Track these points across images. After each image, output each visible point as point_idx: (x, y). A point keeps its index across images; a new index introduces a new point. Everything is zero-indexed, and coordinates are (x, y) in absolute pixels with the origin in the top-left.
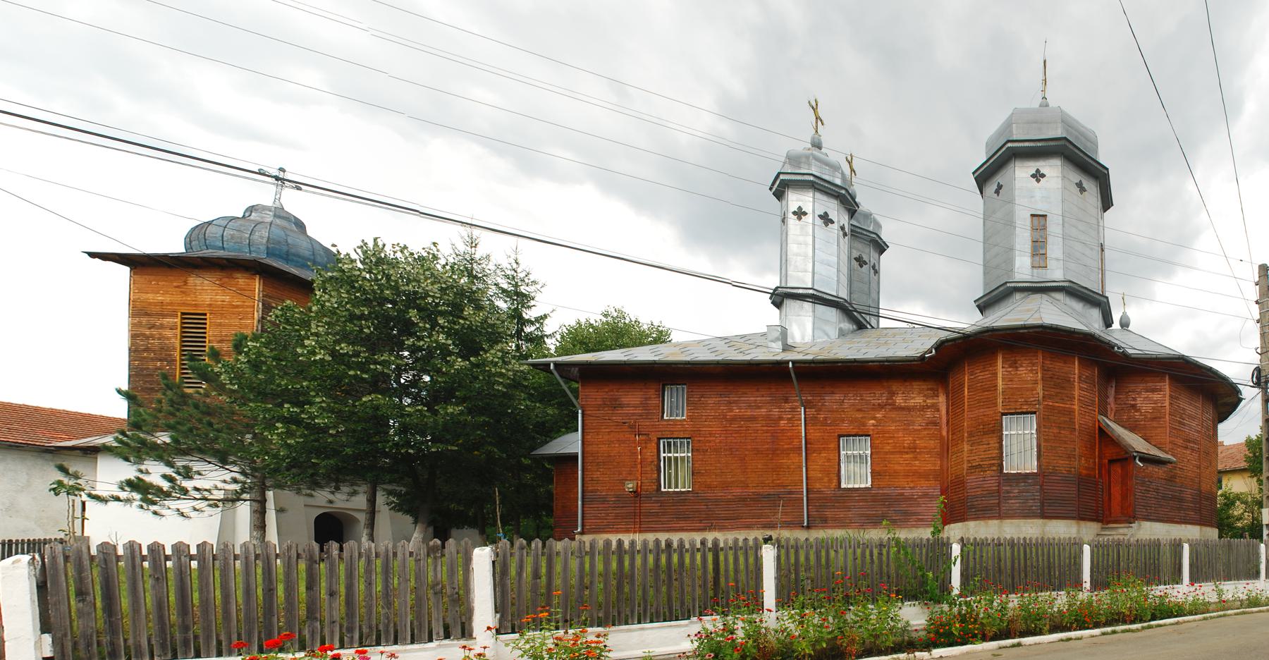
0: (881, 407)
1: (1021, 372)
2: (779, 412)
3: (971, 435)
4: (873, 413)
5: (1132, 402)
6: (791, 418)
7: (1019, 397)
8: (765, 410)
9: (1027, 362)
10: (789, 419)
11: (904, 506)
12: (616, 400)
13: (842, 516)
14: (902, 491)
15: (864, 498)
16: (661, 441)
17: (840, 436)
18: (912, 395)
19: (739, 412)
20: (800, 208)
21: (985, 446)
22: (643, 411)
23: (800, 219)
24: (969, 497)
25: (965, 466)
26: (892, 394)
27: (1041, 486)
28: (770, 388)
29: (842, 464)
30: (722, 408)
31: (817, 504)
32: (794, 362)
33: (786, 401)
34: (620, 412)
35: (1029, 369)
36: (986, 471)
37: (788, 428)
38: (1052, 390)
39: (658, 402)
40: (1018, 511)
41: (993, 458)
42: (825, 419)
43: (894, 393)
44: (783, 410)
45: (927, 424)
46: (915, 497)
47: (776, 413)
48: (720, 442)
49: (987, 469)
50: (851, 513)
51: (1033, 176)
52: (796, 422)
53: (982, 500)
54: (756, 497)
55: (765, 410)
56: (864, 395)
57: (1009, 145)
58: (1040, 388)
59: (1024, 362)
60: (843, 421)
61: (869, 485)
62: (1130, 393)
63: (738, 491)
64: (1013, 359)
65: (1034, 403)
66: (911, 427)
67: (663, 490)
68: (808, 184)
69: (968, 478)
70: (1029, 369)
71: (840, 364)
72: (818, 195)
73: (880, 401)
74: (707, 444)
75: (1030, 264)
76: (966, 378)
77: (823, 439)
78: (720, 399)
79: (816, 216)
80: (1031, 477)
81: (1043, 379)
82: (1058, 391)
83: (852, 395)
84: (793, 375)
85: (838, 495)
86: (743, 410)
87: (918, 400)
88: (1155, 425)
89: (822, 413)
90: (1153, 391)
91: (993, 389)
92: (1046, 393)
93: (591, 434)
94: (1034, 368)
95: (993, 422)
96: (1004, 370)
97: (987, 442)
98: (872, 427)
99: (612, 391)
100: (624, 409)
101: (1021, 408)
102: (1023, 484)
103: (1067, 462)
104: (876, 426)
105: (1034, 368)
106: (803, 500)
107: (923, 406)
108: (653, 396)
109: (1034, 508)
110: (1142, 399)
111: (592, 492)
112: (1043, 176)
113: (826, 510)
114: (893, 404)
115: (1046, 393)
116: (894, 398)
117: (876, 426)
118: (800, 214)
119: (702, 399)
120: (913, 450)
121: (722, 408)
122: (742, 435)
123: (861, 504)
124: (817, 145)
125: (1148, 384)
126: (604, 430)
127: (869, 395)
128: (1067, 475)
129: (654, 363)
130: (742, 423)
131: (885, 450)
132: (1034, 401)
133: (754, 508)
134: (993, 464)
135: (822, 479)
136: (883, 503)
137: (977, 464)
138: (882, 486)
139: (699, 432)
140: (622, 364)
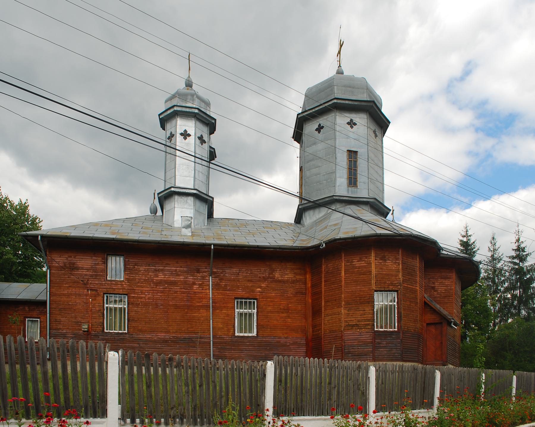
0: (265, 279)
1: (388, 264)
2: (193, 279)
3: (347, 303)
4: (259, 283)
5: (432, 285)
6: (201, 283)
7: (386, 280)
8: (183, 277)
9: (393, 257)
10: (200, 285)
11: (280, 350)
12: (74, 264)
13: (237, 356)
14: (279, 340)
15: (252, 343)
16: (105, 296)
17: (104, 294)
18: (286, 272)
19: (164, 277)
20: (185, 131)
21: (361, 312)
22: (94, 273)
23: (185, 138)
24: (347, 346)
25: (343, 325)
26: (273, 271)
27: (401, 340)
28: (186, 262)
29: (236, 318)
30: (150, 274)
31: (219, 347)
32: (215, 245)
33: (198, 271)
34: (76, 272)
35: (394, 261)
36: (362, 329)
37: (199, 291)
38: (407, 276)
39: (104, 267)
40: (386, 356)
41: (369, 320)
42: (226, 285)
43: (274, 270)
44: (196, 278)
45: (297, 293)
46: (288, 344)
47: (191, 280)
48: (149, 299)
49: (363, 327)
50: (243, 354)
51: (348, 123)
52: (205, 287)
53: (358, 348)
54: (174, 339)
55: (183, 277)
56: (253, 270)
57: (335, 101)
58: (400, 276)
59: (390, 257)
60: (238, 287)
61: (255, 334)
62: (431, 279)
63: (162, 335)
64: (383, 254)
65: (397, 284)
66: (285, 295)
67: (105, 331)
68: (192, 115)
69: (345, 333)
70: (394, 261)
71: (246, 249)
72: (198, 123)
73: (264, 275)
74: (139, 300)
75: (346, 184)
76: (343, 264)
77: (224, 300)
78: (149, 267)
79: (197, 137)
80: (395, 334)
81: (403, 269)
82: (410, 277)
83: (245, 270)
84: (212, 254)
85: (234, 341)
86: (167, 277)
87: (289, 276)
88: (446, 301)
89: (224, 281)
90: (446, 278)
91: (369, 273)
92: (404, 278)
93: (55, 287)
94: (397, 262)
95: (368, 296)
96: (376, 261)
97: (363, 309)
98: (259, 294)
99: (71, 257)
100: (80, 270)
101: (388, 288)
102: (389, 338)
103: (414, 324)
104: (261, 292)
105: (397, 262)
106: (210, 343)
107: (294, 280)
108: (100, 263)
109: (396, 354)
110: (438, 283)
111: (55, 330)
112: (355, 124)
113: (226, 351)
114: (273, 278)
115: (404, 278)
116: (274, 273)
117: (261, 292)
118: (185, 135)
119: (136, 267)
120: (287, 311)
121: (150, 274)
122: (166, 294)
123: (250, 348)
124: (189, 85)
125: (442, 274)
126: (64, 285)
127: (256, 271)
128: (414, 333)
129: (113, 240)
130: (166, 286)
131: (267, 310)
132: (397, 283)
133: (173, 348)
134: (368, 324)
135: (223, 328)
136: (265, 348)
137: (355, 323)
138: (265, 336)
139: (133, 291)
140: (90, 239)
